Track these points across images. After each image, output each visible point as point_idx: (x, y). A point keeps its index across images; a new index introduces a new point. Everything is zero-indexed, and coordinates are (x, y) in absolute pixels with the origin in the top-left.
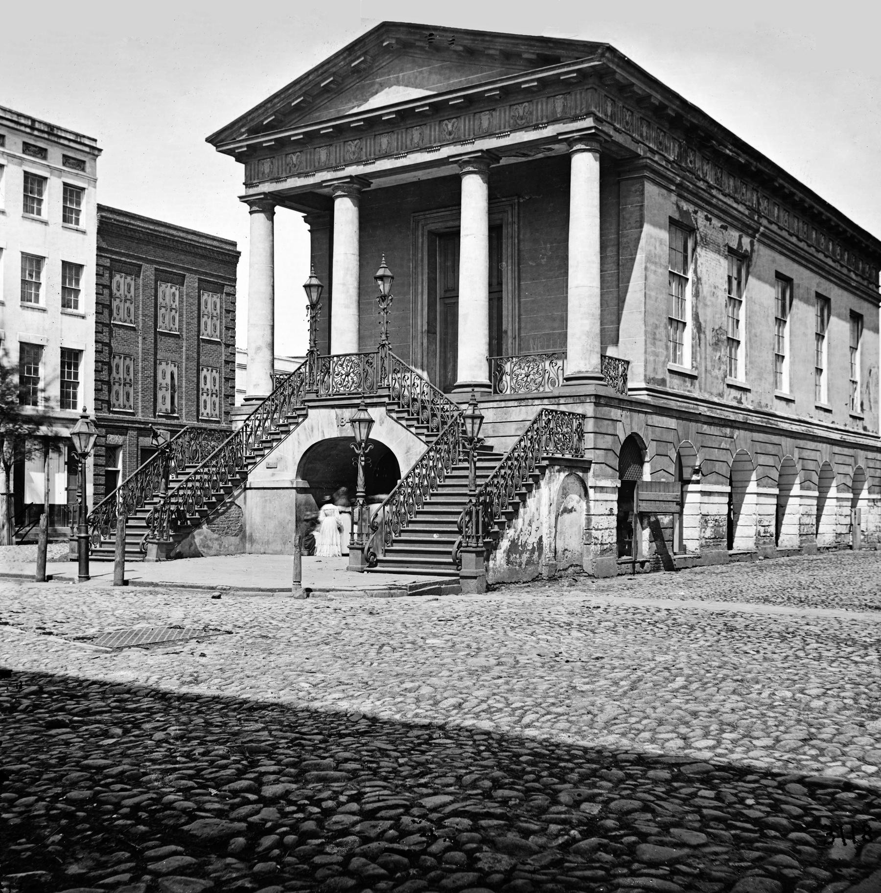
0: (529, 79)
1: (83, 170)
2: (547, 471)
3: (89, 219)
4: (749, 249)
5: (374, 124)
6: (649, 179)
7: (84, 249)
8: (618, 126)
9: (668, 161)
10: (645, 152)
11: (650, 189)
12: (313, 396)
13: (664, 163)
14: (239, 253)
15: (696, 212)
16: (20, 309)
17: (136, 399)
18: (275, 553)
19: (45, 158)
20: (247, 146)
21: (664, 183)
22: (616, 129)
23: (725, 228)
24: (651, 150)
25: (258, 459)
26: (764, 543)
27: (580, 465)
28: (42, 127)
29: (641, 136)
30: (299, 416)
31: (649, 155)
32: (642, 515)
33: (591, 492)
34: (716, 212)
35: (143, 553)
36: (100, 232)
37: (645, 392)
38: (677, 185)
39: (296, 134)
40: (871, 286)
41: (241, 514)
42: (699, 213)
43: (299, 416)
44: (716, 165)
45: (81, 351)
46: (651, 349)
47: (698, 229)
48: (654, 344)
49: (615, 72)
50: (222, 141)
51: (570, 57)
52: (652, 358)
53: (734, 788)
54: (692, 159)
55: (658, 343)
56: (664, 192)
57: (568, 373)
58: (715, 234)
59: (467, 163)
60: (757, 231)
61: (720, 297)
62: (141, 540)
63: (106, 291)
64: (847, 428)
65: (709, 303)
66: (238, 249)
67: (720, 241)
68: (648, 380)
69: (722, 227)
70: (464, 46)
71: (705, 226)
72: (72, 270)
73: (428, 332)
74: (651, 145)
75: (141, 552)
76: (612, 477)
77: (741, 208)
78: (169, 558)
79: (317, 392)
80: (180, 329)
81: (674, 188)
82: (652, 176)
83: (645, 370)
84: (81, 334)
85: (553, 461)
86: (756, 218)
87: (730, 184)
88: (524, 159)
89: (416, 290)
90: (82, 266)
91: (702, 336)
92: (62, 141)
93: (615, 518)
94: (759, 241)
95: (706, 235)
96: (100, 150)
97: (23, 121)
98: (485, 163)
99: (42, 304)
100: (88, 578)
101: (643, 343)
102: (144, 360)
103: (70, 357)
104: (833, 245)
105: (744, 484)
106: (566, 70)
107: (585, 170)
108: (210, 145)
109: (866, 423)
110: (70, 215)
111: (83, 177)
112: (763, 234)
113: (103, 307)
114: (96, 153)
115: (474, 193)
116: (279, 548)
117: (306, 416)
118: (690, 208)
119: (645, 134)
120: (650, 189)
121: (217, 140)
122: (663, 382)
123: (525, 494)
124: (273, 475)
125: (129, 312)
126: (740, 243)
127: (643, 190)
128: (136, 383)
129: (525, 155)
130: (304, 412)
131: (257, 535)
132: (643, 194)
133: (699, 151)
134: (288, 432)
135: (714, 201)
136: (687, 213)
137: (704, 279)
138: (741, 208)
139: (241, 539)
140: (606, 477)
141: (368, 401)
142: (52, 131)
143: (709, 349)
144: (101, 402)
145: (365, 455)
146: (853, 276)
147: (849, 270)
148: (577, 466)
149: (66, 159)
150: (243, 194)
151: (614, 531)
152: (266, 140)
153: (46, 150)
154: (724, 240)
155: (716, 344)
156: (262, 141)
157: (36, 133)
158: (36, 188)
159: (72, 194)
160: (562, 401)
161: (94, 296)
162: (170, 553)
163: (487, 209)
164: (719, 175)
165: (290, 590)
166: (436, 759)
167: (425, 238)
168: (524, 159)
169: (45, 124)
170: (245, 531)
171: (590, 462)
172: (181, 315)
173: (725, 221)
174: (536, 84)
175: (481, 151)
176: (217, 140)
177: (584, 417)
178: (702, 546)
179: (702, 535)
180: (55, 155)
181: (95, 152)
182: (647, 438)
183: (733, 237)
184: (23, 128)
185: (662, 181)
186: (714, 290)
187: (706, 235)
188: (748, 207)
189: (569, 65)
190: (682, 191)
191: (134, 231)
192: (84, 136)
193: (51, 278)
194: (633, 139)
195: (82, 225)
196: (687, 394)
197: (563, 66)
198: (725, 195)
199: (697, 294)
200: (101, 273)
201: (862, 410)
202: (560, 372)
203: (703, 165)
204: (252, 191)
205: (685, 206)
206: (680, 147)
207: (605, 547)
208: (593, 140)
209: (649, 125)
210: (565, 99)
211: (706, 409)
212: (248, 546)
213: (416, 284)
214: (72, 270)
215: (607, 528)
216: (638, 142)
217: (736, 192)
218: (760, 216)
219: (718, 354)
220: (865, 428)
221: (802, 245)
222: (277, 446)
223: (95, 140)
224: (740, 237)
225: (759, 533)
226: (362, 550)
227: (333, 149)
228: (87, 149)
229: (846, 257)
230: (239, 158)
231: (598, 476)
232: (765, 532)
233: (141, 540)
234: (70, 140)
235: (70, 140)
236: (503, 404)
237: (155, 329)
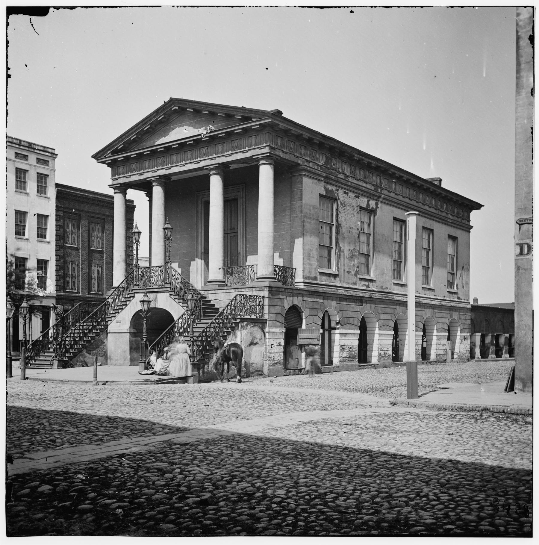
0: (238, 129)
1: (48, 165)
2: (240, 325)
3: (52, 192)
4: (374, 207)
5: (169, 150)
6: (305, 175)
7: (49, 206)
8: (285, 150)
9: (318, 165)
10: (303, 162)
11: (305, 180)
12: (137, 287)
13: (316, 167)
14: (135, 207)
15: (337, 190)
16: (15, 240)
17: (78, 285)
18: (120, 365)
19: (27, 160)
20: (111, 160)
21: (317, 177)
22: (283, 152)
23: (358, 197)
24: (307, 161)
25: (113, 318)
26: (384, 359)
27: (261, 321)
28: (25, 144)
29: (301, 154)
30: (130, 297)
31: (306, 164)
32: (301, 346)
33: (267, 334)
34: (351, 189)
35: (52, 365)
36: (58, 198)
37: (303, 284)
38: (325, 177)
39: (133, 154)
40: (464, 221)
41: (105, 346)
42: (340, 191)
43: (130, 297)
44: (351, 165)
45: (48, 260)
46: (307, 262)
47: (339, 199)
48: (309, 259)
49: (279, 125)
50: (100, 157)
51: (255, 118)
52: (308, 266)
53: (226, 469)
54: (335, 162)
55: (311, 259)
56: (316, 181)
57: (259, 276)
58: (351, 200)
59: (212, 169)
60: (380, 197)
61: (354, 233)
62: (51, 359)
63: (62, 230)
64: (445, 298)
65: (346, 236)
66: (134, 204)
67: (355, 205)
68: (304, 277)
69: (355, 196)
70: (209, 111)
71: (344, 197)
72: (42, 218)
73: (204, 253)
74: (307, 158)
75: (51, 364)
76: (280, 326)
77: (368, 186)
78: (64, 367)
79: (139, 285)
80: (102, 248)
81: (322, 179)
82: (307, 174)
83: (303, 273)
84: (48, 251)
85: (243, 320)
86: (379, 190)
87: (360, 174)
88: (247, 165)
89: (198, 232)
90: (48, 216)
91: (342, 254)
92: (36, 151)
93: (282, 347)
94: (381, 202)
95: (344, 202)
96: (57, 155)
97: (15, 141)
98: (224, 170)
99: (27, 236)
100: (11, 376)
101: (302, 259)
102: (82, 264)
103: (42, 264)
104: (435, 201)
105: (373, 329)
106: (255, 124)
107: (266, 174)
108: (93, 159)
109: (460, 295)
110: (41, 189)
111: (48, 169)
112: (384, 199)
113: (61, 237)
114: (55, 156)
115: (216, 184)
116: (122, 363)
117: (134, 297)
118: (334, 188)
119: (303, 153)
120: (305, 180)
121: (97, 156)
122: (316, 278)
123: (226, 336)
124: (119, 326)
125: (74, 239)
126: (368, 204)
127: (302, 182)
128: (78, 276)
129: (247, 163)
130: (133, 295)
131: (113, 356)
132: (302, 184)
133: (340, 159)
134: (126, 305)
135: (349, 184)
136: (332, 191)
137: (343, 224)
138: (368, 186)
139: (105, 358)
140: (276, 327)
141: (147, 290)
142: (30, 146)
143: (347, 261)
144: (59, 287)
145: (146, 317)
146: (451, 217)
147: (447, 214)
148: (261, 323)
149: (38, 160)
150: (111, 184)
151: (282, 354)
152: (120, 157)
153: (27, 156)
154: (357, 203)
155: (351, 257)
156: (121, 154)
157: (22, 147)
158: (22, 176)
159: (42, 178)
160: (254, 289)
161: (55, 231)
162: (64, 365)
163: (222, 192)
164: (353, 170)
165: (92, 382)
166: (277, 476)
167: (203, 204)
168: (247, 165)
169: (27, 142)
170: (107, 354)
171: (266, 320)
172: (103, 240)
173: (357, 193)
174: (241, 131)
175: (218, 164)
176: (97, 156)
177: (264, 297)
178: (340, 361)
179: (341, 355)
180: (32, 158)
181: (54, 155)
182: (303, 307)
183: (363, 202)
184: (14, 145)
185: (314, 175)
186: (349, 229)
187: (344, 202)
188: (373, 185)
189: (255, 121)
190: (328, 180)
191: (76, 196)
192: (48, 148)
193: (31, 224)
194: (295, 156)
195: (49, 195)
196: (331, 284)
197: (253, 122)
198: (358, 180)
199: (337, 233)
200: (58, 219)
201: (457, 288)
202: (256, 275)
203: (342, 166)
204: (115, 182)
205: (330, 187)
206: (327, 157)
207: (276, 362)
208: (270, 158)
209: (306, 148)
210: (256, 138)
211: (343, 291)
212: (108, 361)
213: (198, 228)
214: (42, 218)
215: (278, 353)
216: (298, 157)
217: (365, 177)
218: (382, 189)
219: (353, 263)
220: (459, 298)
221: (412, 202)
222: (121, 312)
223: (54, 150)
224: (368, 201)
225: (380, 355)
226: (145, 363)
227: (151, 161)
228: (50, 155)
229: (445, 206)
230: (109, 165)
231: (271, 327)
232: (384, 354)
233: (51, 359)
234: (40, 150)
235: (40, 150)
236: (228, 291)
237: (89, 248)
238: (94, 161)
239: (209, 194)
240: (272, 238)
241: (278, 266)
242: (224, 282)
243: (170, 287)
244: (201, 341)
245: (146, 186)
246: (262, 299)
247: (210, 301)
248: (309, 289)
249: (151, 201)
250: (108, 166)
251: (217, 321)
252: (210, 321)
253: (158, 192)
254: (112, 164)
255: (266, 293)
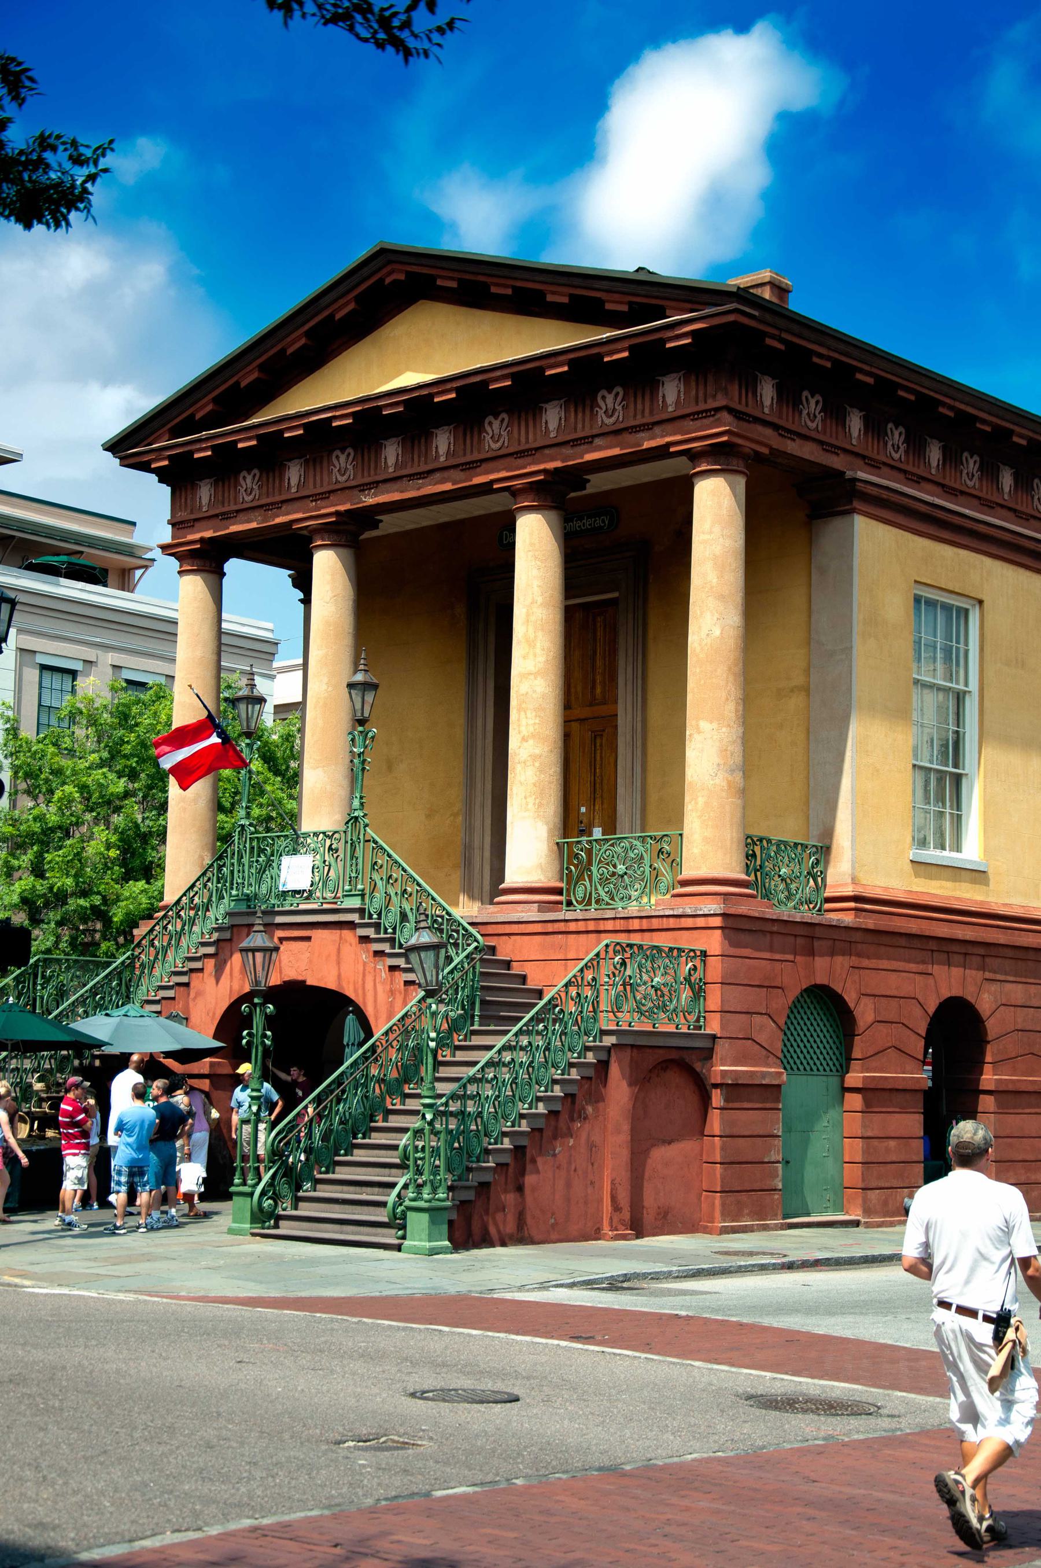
120: (862, 525)
171: (714, 1037)
230: (163, 476)
238: (111, 461)
239: (513, 577)
240: (977, 886)
241: (761, 840)
242: (559, 891)
243: (361, 911)
244: (462, 1114)
245: (290, 552)
246: (698, 962)
247: (508, 964)
248: (870, 923)
249: (307, 601)
250: (161, 481)
251: (524, 1041)
252: (501, 1041)
253: (327, 566)
254: (178, 476)
255: (714, 942)
